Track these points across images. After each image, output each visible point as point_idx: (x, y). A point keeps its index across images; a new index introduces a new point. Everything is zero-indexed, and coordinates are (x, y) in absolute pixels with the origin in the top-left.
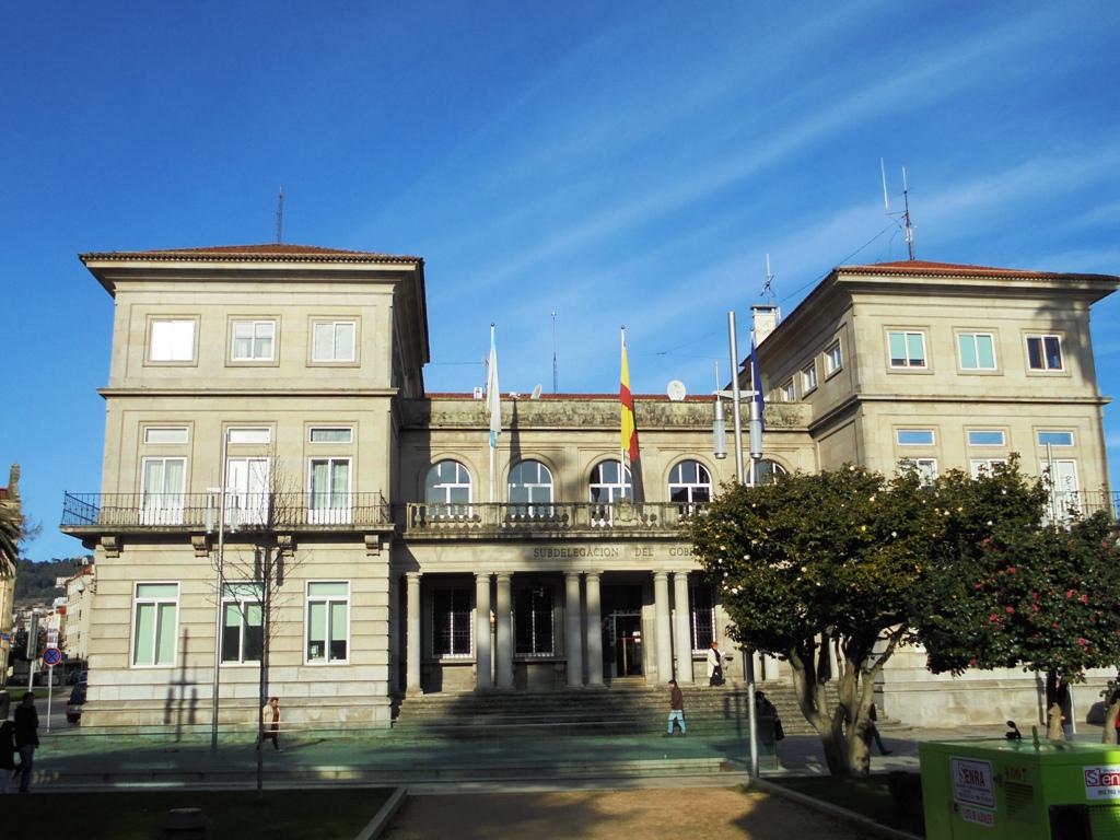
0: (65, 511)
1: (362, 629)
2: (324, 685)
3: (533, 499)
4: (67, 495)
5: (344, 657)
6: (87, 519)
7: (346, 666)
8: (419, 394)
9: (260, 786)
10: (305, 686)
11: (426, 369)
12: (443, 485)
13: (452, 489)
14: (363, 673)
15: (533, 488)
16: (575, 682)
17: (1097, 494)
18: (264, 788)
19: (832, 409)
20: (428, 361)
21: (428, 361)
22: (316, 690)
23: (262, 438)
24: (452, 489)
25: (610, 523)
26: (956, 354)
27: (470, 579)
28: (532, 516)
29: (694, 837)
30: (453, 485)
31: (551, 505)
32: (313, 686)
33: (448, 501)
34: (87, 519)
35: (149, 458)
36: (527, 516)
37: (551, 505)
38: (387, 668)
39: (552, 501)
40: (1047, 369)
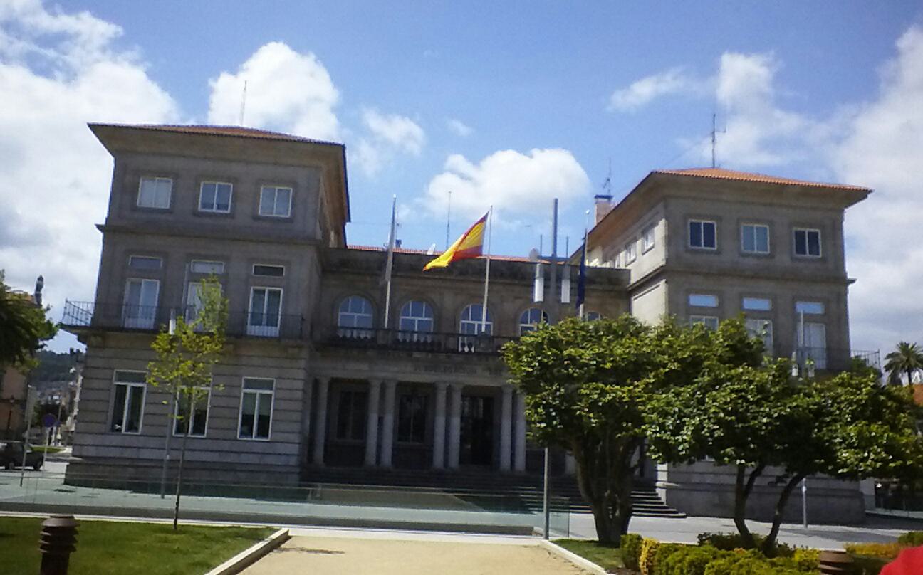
3: (494, 333)
4: (67, 302)
5: (267, 436)
7: (267, 442)
8: (343, 246)
11: (348, 226)
12: (426, 319)
13: (419, 321)
15: (358, 317)
16: (371, 458)
21: (349, 221)
23: (219, 269)
24: (419, 321)
26: (491, 220)
27: (365, 383)
29: (781, 571)
30: (420, 319)
32: (143, 451)
33: (416, 329)
34: (81, 321)
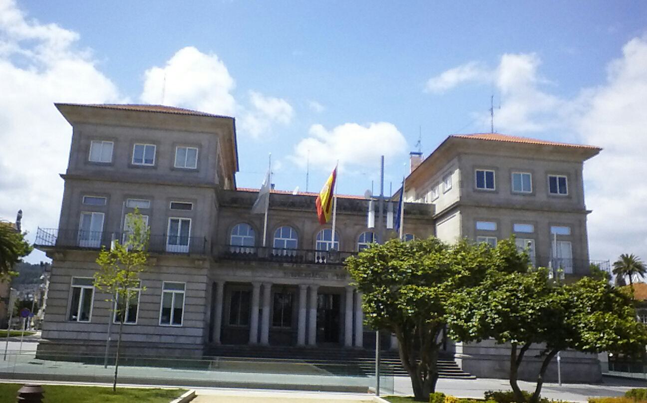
0: (37, 237)
1: (191, 309)
2: (168, 337)
3: (340, 249)
4: (39, 228)
6: (48, 242)
7: (181, 327)
8: (234, 189)
9: (115, 385)
10: (158, 337)
11: (237, 174)
14: (189, 332)
16: (253, 338)
17: (55, 230)
18: (113, 384)
19: (445, 208)
20: (238, 170)
22: (164, 339)
25: (325, 261)
27: (250, 285)
28: (275, 255)
31: (284, 249)
35: (173, 218)
36: (282, 255)
37: (284, 249)
38: (462, 348)
39: (285, 247)
40: (485, 189)
